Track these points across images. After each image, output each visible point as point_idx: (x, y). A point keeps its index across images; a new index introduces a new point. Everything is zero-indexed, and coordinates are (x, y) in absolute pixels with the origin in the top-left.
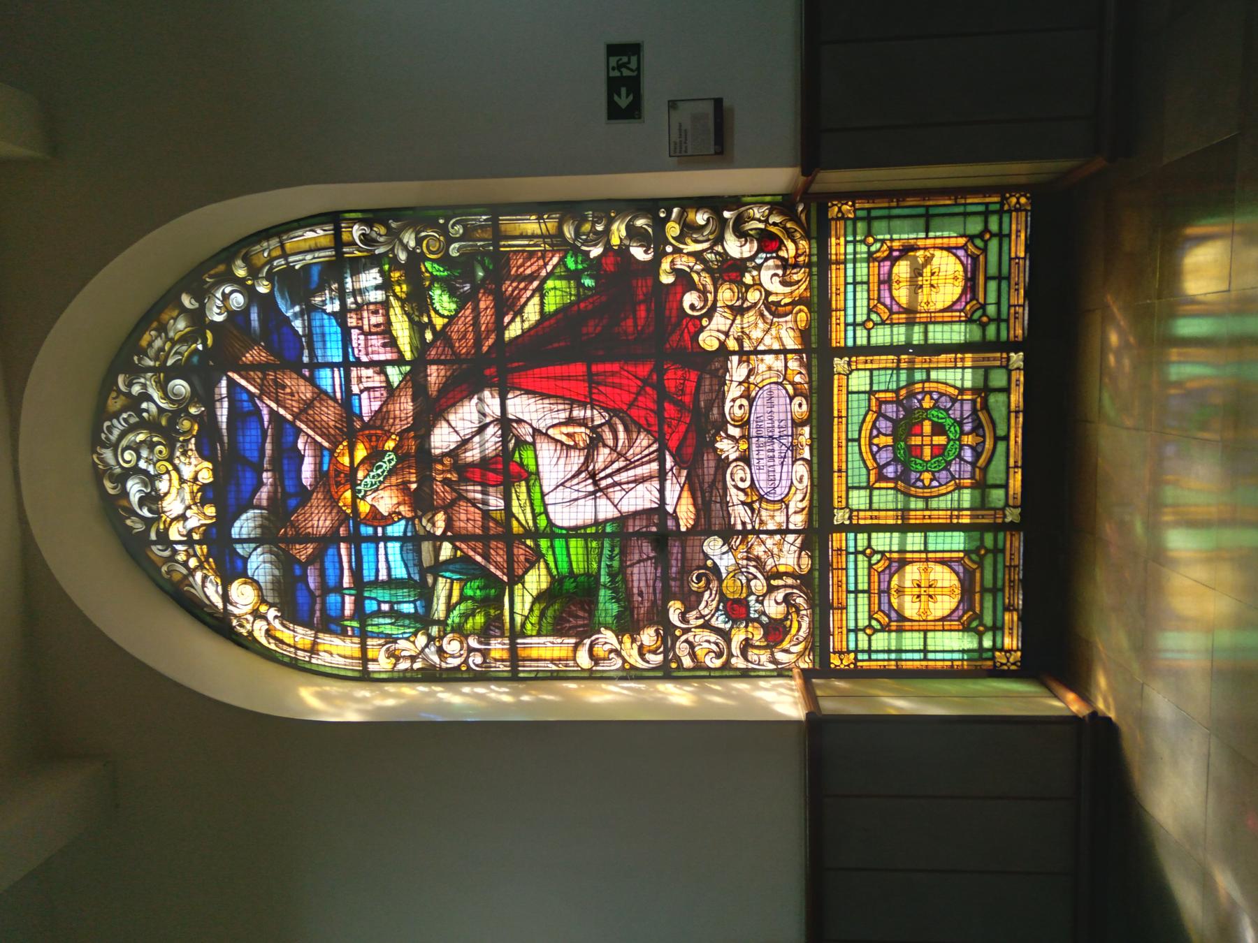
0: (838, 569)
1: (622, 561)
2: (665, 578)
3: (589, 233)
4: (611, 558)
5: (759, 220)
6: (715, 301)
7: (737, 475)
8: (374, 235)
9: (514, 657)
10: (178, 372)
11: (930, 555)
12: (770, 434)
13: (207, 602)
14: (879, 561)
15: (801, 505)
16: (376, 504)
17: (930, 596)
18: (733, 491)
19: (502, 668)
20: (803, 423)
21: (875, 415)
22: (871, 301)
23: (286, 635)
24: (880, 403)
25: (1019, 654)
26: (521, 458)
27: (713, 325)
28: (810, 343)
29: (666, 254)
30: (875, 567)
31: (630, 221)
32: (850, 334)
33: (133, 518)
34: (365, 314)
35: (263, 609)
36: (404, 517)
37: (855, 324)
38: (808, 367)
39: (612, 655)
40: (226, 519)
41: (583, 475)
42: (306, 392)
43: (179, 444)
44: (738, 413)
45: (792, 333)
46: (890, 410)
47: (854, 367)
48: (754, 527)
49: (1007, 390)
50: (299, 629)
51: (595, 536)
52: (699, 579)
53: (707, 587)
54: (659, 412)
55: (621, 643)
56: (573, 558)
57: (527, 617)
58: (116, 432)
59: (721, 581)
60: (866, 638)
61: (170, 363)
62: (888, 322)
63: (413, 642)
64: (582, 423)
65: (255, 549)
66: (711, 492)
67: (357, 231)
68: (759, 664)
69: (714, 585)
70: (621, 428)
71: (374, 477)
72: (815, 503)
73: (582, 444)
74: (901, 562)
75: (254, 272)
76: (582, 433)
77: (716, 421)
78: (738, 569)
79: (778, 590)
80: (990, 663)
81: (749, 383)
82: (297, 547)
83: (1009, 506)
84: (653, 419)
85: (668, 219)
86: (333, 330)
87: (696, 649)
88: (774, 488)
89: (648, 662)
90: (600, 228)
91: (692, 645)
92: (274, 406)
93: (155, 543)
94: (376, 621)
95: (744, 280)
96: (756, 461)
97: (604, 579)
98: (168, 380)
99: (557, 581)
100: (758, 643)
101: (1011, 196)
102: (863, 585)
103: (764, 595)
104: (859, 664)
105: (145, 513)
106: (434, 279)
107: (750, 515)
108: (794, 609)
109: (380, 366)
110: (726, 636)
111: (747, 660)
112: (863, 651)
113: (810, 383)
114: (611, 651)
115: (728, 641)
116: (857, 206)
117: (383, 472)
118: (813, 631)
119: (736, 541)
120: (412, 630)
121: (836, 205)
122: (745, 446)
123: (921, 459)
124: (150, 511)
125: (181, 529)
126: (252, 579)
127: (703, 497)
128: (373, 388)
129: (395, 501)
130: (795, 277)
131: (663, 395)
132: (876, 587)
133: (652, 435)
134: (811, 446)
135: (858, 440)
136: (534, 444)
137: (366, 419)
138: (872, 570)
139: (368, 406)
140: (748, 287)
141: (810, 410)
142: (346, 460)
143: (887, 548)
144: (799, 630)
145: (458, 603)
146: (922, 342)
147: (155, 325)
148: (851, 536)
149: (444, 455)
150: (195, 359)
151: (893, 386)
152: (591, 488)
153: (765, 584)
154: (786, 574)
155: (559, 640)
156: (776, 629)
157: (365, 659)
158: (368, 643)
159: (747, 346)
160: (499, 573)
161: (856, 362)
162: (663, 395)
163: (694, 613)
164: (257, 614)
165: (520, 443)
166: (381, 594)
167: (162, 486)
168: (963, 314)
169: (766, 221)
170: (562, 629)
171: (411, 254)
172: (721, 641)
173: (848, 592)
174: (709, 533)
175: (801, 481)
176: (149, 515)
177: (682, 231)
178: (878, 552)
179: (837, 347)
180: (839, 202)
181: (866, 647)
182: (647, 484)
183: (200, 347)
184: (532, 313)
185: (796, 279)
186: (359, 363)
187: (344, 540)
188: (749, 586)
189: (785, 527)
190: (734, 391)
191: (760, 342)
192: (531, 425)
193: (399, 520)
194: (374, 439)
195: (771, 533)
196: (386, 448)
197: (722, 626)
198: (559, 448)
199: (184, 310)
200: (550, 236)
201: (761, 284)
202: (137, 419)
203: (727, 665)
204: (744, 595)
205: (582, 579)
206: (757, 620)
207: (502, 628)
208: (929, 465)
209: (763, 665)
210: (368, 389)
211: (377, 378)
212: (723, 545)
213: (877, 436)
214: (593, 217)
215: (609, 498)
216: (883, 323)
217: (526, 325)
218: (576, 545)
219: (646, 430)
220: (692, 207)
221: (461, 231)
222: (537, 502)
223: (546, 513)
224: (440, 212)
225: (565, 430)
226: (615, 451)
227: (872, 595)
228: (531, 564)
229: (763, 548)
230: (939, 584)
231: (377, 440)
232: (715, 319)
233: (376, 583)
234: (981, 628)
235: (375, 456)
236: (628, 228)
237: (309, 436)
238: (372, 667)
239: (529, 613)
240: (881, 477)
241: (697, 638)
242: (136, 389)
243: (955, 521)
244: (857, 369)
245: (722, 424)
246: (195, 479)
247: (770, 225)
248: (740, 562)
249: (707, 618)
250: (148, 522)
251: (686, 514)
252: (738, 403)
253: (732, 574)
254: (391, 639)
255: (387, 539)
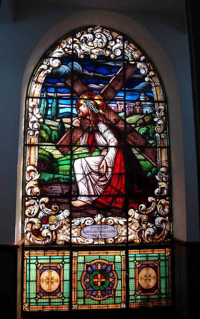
0: (58, 253)
1: (62, 183)
2: (56, 197)
3: (162, 176)
4: (63, 179)
5: (165, 227)
6: (143, 214)
7: (89, 221)
8: (161, 112)
9: (31, 145)
10: (123, 53)
11: (62, 282)
12: (102, 231)
13: (54, 53)
14: (60, 266)
15: (79, 241)
16: (83, 106)
17: (48, 283)
18: (85, 219)
19: (28, 141)
20: (105, 242)
21: (108, 264)
22: (142, 262)
23: (42, 74)
24: (112, 265)
25: (28, 311)
26: (96, 151)
27: (136, 213)
28: (129, 244)
29: (156, 199)
30: (58, 265)
31: (166, 188)
32: (132, 256)
33: (81, 34)
34: (139, 107)
35: (51, 68)
36: (78, 114)
37: (135, 257)
38: (123, 243)
39: (30, 177)
40: (79, 61)
41: (91, 171)
42: (117, 88)
43: (102, 50)
44: (109, 222)
45: (133, 238)
46: (109, 269)
47: (122, 257)
48: (73, 226)
49: (115, 303)
50: (44, 79)
51: (71, 173)
52: (56, 208)
53: (53, 211)
54: (109, 195)
55: (35, 180)
56: (65, 166)
57: (45, 150)
58: (106, 33)
59: (55, 215)
60: (34, 262)
61: (125, 50)
62: (136, 267)
63: (38, 113)
64: (107, 171)
65: (70, 68)
66: (84, 212)
67: (162, 107)
68: (26, 227)
69: (53, 213)
70: (105, 183)
71: (91, 106)
72: (80, 246)
73: (100, 170)
74: (59, 271)
75: (151, 77)
76: (103, 171)
77: (107, 214)
78: (58, 221)
79: (51, 234)
80: (25, 302)
81: (118, 225)
82: (70, 81)
83: (78, 306)
84: (108, 193)
85: (166, 200)
86: (135, 98)
87: (32, 206)
88: (85, 233)
89: (28, 189)
90: (164, 179)
91: (33, 205)
92: (113, 78)
93: (73, 40)
94: (45, 103)
95: (149, 223)
96: (94, 227)
97: (56, 176)
98: (121, 49)
99: (56, 160)
100: (33, 227)
101: (171, 301)
102: (52, 261)
103: (49, 229)
104: (25, 260)
105: (82, 38)
106: (149, 129)
107: (77, 225)
108: (44, 239)
109: (124, 110)
110: (36, 216)
111: (28, 223)
112: (30, 261)
113: (118, 244)
114: (32, 177)
115: (34, 217)
116: (169, 256)
117: (93, 108)
118: (37, 245)
119: (67, 220)
120: (42, 113)
121: (169, 250)
122: (98, 223)
123: (94, 278)
124: (83, 40)
125: (77, 48)
126: (60, 66)
127: (83, 210)
128: (118, 108)
129: (83, 111)
130: (149, 239)
131: (115, 197)
132: (51, 265)
133: (103, 193)
134: (98, 244)
135: (100, 259)
136: (100, 155)
137: (109, 105)
138: (57, 264)
139: (113, 106)
140: (147, 224)
141: (110, 244)
142: (96, 98)
143: (64, 268)
144: (37, 240)
145: (50, 128)
146: (129, 277)
147: (136, 48)
148: (69, 257)
149: (98, 127)
150: (126, 58)
151: (116, 269)
152: (86, 173)
153: (53, 230)
154: (56, 237)
155: (36, 160)
156: (38, 233)
157: (33, 98)
158: (38, 99)
159: (129, 224)
160: (60, 142)
161: (124, 258)
162: (115, 197)
163: (44, 206)
164: (49, 67)
165: (101, 151)
166: (54, 104)
167: (90, 44)
168: (138, 289)
169: (165, 230)
170: (40, 161)
171: (156, 122)
172: (34, 214)
173: (50, 256)
174: (71, 212)
175: (87, 241)
176: (81, 39)
177: (163, 204)
178: (63, 266)
179: (128, 252)
180: (170, 251)
181: (31, 262)
182: (87, 191)
183: (130, 60)
184: (140, 157)
185: (149, 239)
186: (125, 104)
187: (72, 95)
188: (52, 224)
189: (72, 236)
190: (116, 220)
191: (130, 228)
192: (106, 154)
193: (78, 112)
194: (103, 107)
195: (70, 231)
196: (100, 110)
197: (39, 215)
198: (99, 163)
199: (140, 57)
200: (161, 163)
201: (147, 228)
202: (109, 40)
203: (26, 216)
204: (50, 223)
205: (57, 169)
206: (41, 227)
207: (41, 142)
208: (92, 281)
209: (26, 228)
210: (118, 106)
211: (121, 109)
212: (67, 216)
213: (101, 265)
214: (167, 177)
215: (83, 178)
216: (136, 265)
217: (136, 155)
218: (67, 167)
219: (104, 191)
220: (169, 207)
221: (162, 137)
222: (82, 155)
223: (79, 158)
224: (168, 132)
225: (105, 166)
226: (98, 181)
227: (49, 264)
228: (62, 152)
229: (65, 229)
230: (54, 279)
231: (102, 108)
232: (137, 214)
233: (58, 104)
234: (37, 299)
235: (97, 106)
236: (164, 188)
237: (104, 87)
238: (30, 100)
239: (46, 151)
240: (88, 266)
241: (35, 207)
242: (118, 41)
243: (73, 289)
244: (122, 258)
245: (106, 216)
246: (92, 53)
247: (164, 231)
248: (61, 221)
249: (42, 210)
250: (79, 39)
251: (77, 203)
252: (112, 221)
253: (57, 219)
254: (39, 106)
255: (72, 108)
